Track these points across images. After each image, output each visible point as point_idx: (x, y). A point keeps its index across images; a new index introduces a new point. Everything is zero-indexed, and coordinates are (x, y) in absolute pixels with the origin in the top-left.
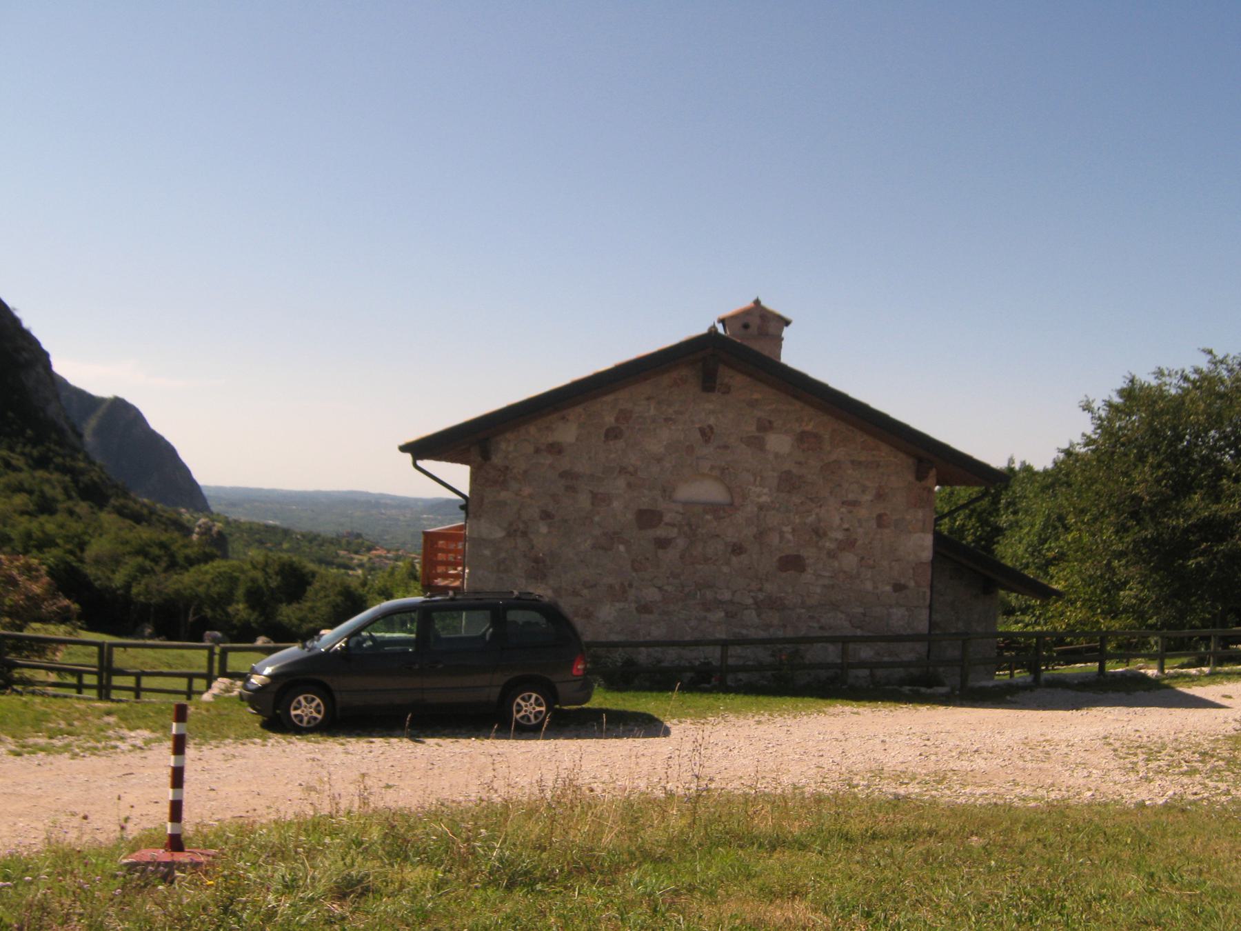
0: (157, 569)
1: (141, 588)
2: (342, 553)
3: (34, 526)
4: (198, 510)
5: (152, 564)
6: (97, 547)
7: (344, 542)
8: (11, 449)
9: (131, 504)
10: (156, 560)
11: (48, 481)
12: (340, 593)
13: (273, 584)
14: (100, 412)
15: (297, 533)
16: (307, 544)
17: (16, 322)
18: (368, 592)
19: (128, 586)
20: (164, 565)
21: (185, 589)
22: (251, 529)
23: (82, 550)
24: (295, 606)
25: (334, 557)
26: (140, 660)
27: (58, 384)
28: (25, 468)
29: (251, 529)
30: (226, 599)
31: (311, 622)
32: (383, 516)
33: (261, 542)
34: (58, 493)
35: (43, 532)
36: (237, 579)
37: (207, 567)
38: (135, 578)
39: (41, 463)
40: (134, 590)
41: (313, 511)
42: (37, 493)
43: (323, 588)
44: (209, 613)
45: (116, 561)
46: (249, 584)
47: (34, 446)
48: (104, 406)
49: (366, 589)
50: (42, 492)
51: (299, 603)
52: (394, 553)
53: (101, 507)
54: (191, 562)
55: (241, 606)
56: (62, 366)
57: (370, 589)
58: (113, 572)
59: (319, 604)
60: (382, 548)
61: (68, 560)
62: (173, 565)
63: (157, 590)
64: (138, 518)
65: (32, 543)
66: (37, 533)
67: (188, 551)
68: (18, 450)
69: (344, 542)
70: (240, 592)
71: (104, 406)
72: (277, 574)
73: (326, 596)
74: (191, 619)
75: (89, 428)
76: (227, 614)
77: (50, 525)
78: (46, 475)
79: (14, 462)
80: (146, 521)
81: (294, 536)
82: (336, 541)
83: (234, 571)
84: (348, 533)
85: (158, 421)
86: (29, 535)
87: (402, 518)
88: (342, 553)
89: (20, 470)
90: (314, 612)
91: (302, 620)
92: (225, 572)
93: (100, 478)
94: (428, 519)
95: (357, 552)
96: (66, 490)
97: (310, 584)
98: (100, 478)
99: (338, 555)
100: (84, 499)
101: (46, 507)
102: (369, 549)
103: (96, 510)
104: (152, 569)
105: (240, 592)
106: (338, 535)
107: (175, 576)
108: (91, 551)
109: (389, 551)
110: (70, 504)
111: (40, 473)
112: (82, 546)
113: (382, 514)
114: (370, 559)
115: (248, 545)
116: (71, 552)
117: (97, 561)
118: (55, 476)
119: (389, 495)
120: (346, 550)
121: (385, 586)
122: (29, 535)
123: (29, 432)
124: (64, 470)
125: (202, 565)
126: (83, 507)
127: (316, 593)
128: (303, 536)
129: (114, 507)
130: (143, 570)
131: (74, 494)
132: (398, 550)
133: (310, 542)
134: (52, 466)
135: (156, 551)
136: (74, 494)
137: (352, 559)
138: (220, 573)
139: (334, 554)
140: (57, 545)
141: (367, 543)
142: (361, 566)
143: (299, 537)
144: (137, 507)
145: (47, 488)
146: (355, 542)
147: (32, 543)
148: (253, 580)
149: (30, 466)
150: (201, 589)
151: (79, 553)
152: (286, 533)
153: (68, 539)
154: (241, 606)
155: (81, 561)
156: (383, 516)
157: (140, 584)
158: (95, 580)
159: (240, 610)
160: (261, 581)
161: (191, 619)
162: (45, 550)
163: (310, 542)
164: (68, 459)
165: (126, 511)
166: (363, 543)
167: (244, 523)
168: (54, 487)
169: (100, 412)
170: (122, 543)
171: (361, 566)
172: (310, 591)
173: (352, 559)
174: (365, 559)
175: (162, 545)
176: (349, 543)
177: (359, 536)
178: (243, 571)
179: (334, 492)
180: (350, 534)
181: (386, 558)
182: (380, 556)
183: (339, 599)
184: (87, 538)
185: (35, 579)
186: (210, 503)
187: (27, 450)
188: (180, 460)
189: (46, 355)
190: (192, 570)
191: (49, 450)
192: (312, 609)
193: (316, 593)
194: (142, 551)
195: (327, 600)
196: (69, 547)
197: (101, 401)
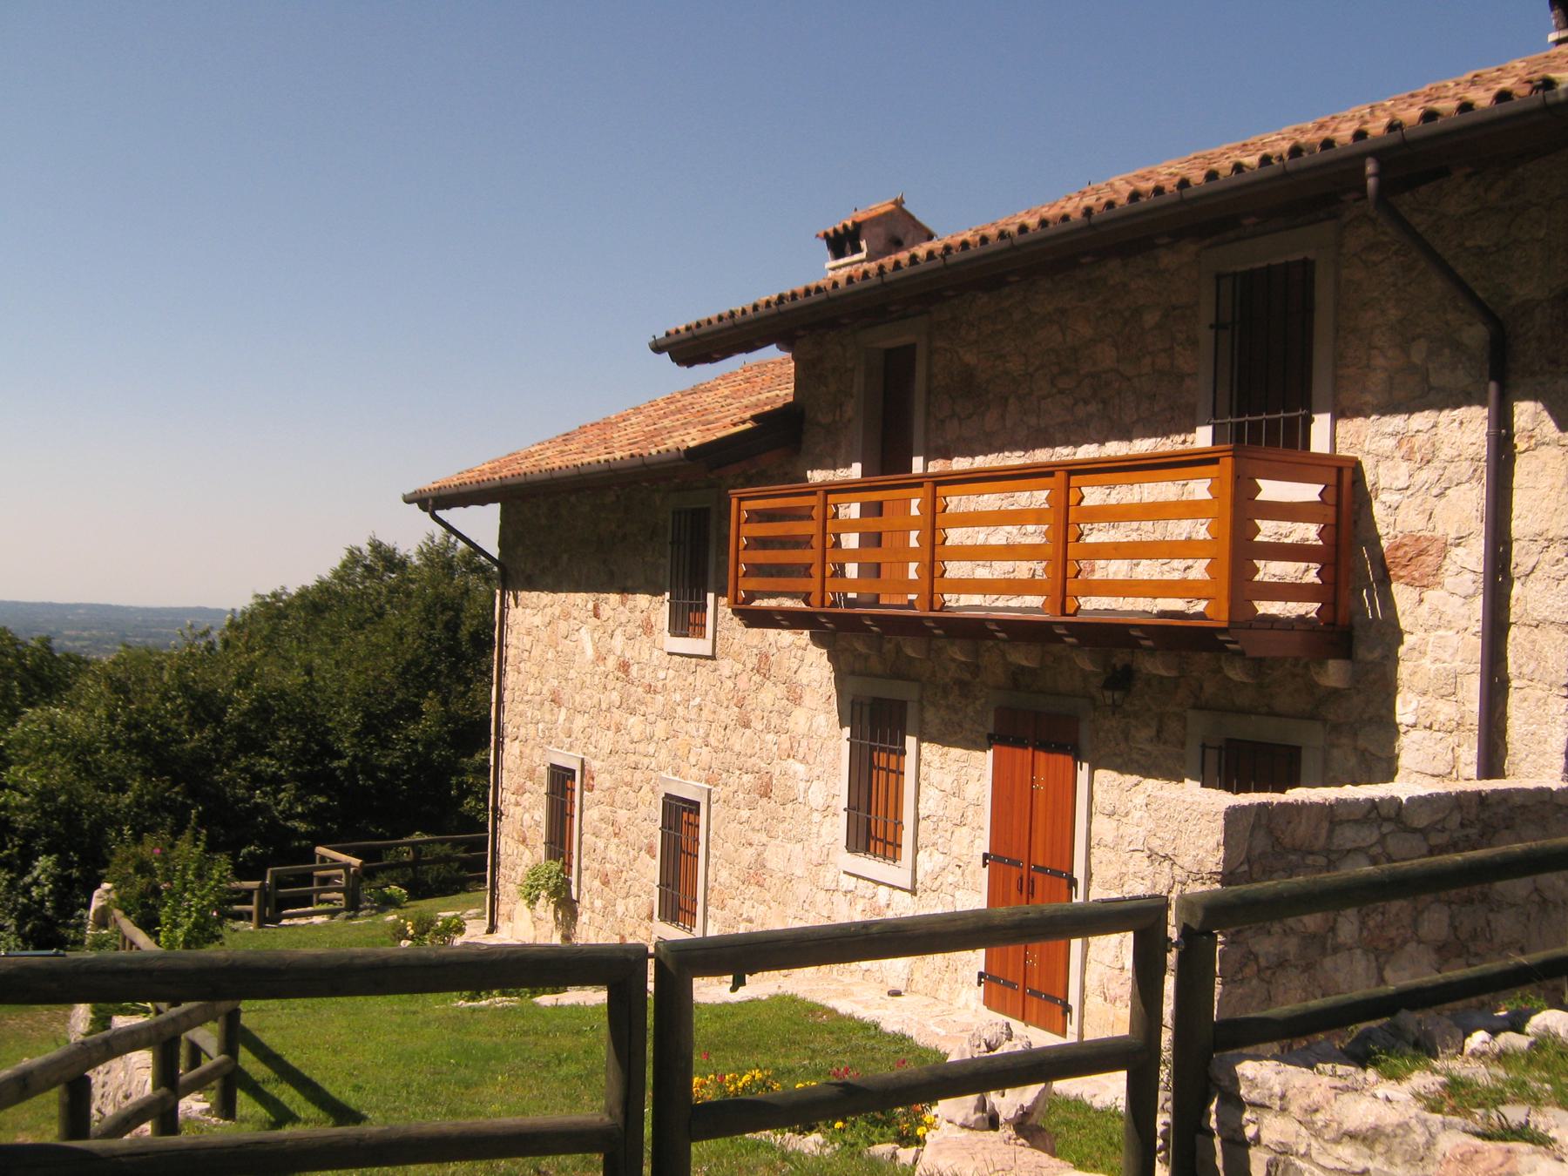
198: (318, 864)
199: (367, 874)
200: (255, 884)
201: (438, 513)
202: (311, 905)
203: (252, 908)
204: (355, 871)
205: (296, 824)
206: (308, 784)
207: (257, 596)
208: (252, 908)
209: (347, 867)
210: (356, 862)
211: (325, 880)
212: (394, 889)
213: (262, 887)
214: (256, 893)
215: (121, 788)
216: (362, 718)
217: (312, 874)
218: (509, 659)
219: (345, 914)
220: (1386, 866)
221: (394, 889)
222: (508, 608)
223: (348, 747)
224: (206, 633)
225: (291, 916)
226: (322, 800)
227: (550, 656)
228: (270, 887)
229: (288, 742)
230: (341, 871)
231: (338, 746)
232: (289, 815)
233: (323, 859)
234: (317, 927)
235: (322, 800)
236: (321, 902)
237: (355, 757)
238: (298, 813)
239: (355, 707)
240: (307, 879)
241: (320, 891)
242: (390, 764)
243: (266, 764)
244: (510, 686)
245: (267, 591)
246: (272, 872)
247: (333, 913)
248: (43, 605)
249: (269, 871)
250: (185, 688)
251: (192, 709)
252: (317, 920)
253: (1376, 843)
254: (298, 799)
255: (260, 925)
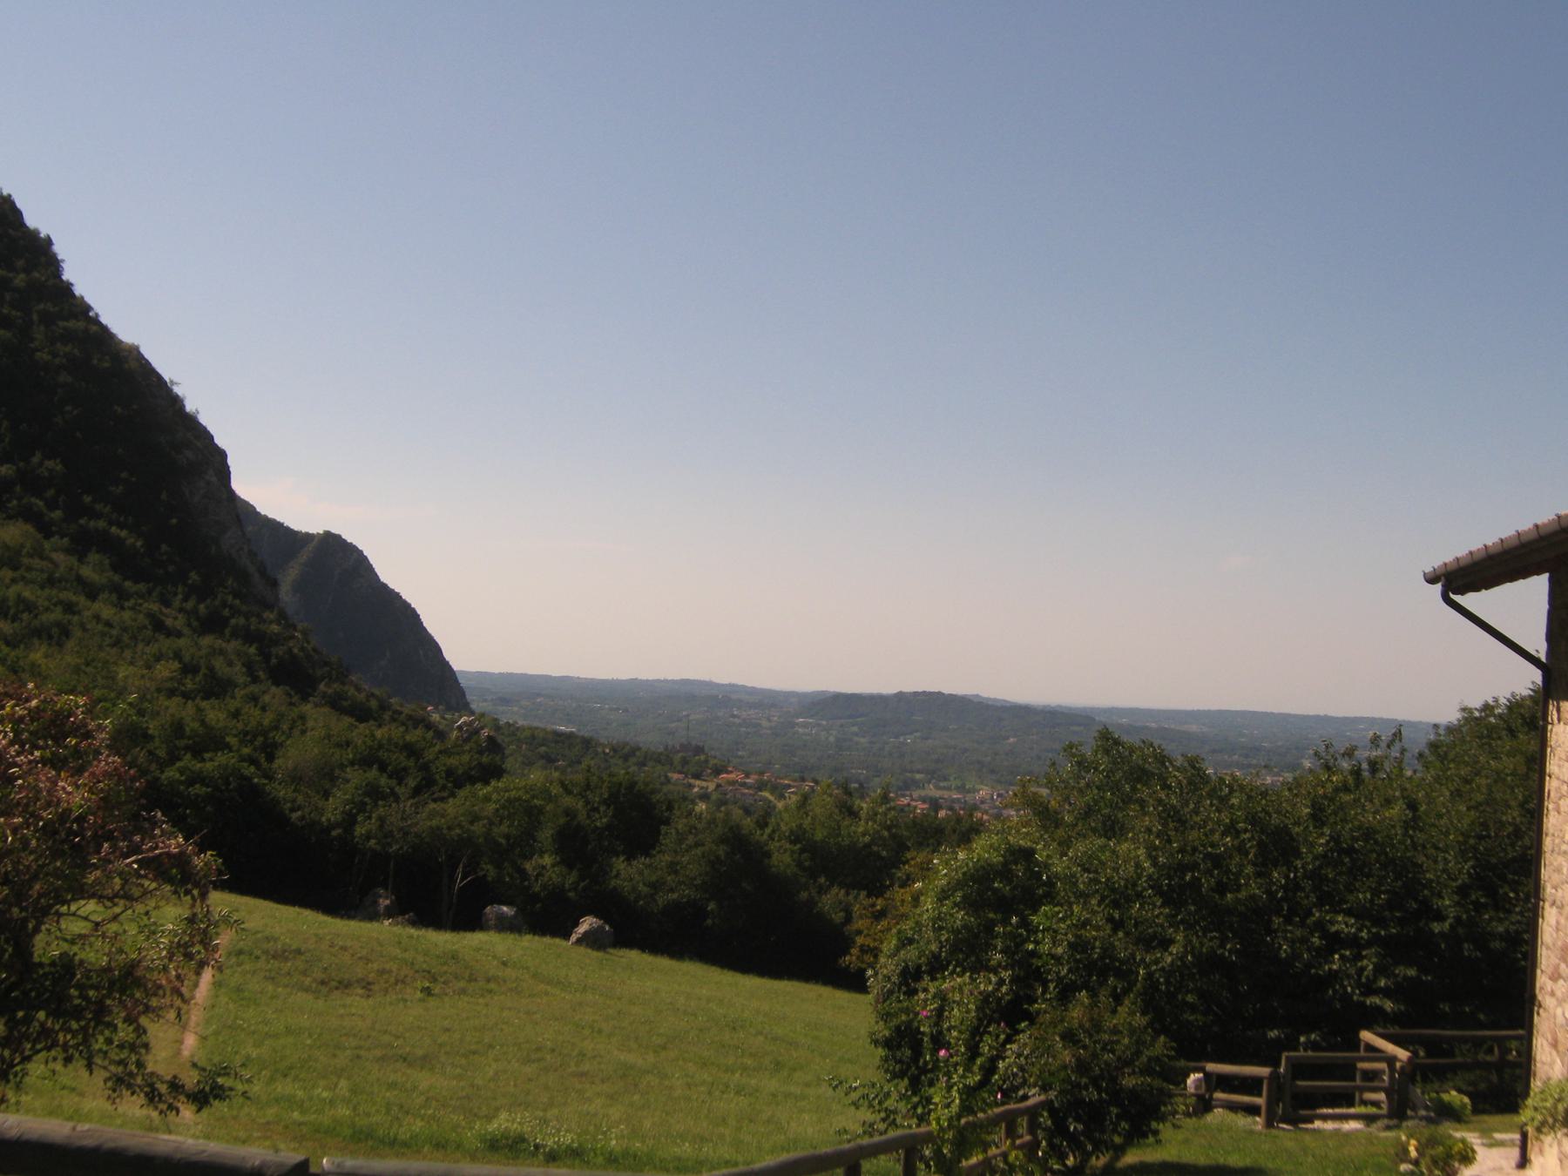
0: (399, 790)
1: (372, 825)
2: (675, 776)
3: (186, 712)
4: (449, 708)
5: (393, 782)
6: (298, 753)
7: (677, 758)
8: (166, 603)
9: (352, 691)
10: (399, 775)
11: (222, 652)
12: (723, 840)
13: (602, 821)
14: (304, 556)
15: (604, 746)
16: (620, 762)
17: (176, 402)
18: (771, 837)
19: (349, 821)
20: (412, 783)
21: (449, 828)
22: (533, 737)
23: (271, 758)
24: (642, 861)
25: (662, 784)
26: (375, 966)
27: (243, 513)
28: (186, 631)
29: (533, 737)
30: (524, 843)
31: (672, 890)
32: (736, 720)
33: (550, 760)
34: (237, 673)
35: (203, 722)
36: (541, 810)
37: (483, 791)
38: (361, 807)
39: (212, 624)
40: (359, 830)
41: (626, 711)
42: (203, 671)
43: (692, 829)
44: (489, 870)
45: (327, 777)
46: (562, 821)
47: (201, 600)
48: (311, 547)
49: (768, 831)
50: (211, 669)
51: (647, 855)
52: (756, 777)
53: (305, 698)
54: (458, 780)
55: (547, 860)
56: (242, 485)
57: (774, 831)
58: (326, 795)
59: (685, 859)
60: (736, 768)
61: (246, 772)
62: (426, 785)
63: (401, 829)
64: (361, 714)
65: (182, 743)
66: (192, 725)
67: (453, 761)
68: (177, 602)
69: (677, 758)
70: (546, 835)
71: (311, 547)
72: (606, 802)
73: (697, 845)
74: (459, 884)
75: (288, 577)
76: (522, 873)
77: (215, 714)
78: (219, 643)
79: (169, 622)
80: (375, 720)
81: (600, 750)
82: (663, 758)
83: (534, 797)
84: (682, 745)
85: (392, 571)
86: (178, 728)
87: (765, 723)
88: (675, 776)
89: (179, 635)
90: (676, 872)
91: (656, 886)
92: (519, 799)
93: (302, 649)
94: (805, 725)
95: (697, 776)
96: (249, 667)
97: (667, 822)
98: (302, 649)
99: (668, 781)
100: (277, 684)
101: (216, 688)
102: (717, 771)
103: (295, 699)
104: (393, 793)
105: (546, 835)
106: (666, 748)
107: (432, 805)
108: (284, 763)
109: (747, 776)
110: (254, 688)
111: (207, 641)
112: (270, 751)
113: (734, 716)
114: (719, 786)
115: (529, 763)
116: (253, 761)
117: (296, 778)
118: (234, 645)
119: (744, 687)
120: (680, 772)
121: (800, 826)
122: (178, 728)
123: (194, 576)
124: (249, 637)
125: (478, 786)
126: (275, 695)
127: (681, 839)
128: (614, 750)
129: (324, 695)
130: (374, 793)
131: (261, 674)
132: (762, 773)
133: (626, 758)
134: (227, 631)
135: (400, 759)
136: (261, 674)
137: (691, 786)
138: (509, 801)
139: (663, 778)
140: (228, 747)
141: (712, 762)
142: (705, 797)
143: (607, 751)
144: (362, 697)
145: (218, 663)
146: (695, 760)
147: (182, 743)
148: (569, 813)
149: (195, 631)
150: (478, 828)
151: (265, 765)
152: (587, 743)
153: (246, 736)
154: (547, 860)
155: (270, 778)
156: (736, 720)
157: (370, 818)
158: (293, 810)
159: (545, 865)
160: (582, 817)
161: (459, 884)
162: (207, 756)
163: (626, 758)
164: (253, 620)
165: (345, 704)
166: (706, 761)
167: (523, 729)
168: (230, 664)
169: (304, 556)
170: (339, 745)
171: (705, 797)
172: (668, 836)
173: (691, 786)
174: (712, 786)
175: (411, 750)
176: (685, 762)
177: (699, 750)
178: (550, 798)
179: (659, 681)
180: (684, 747)
181: (744, 785)
182: (733, 783)
183: (722, 851)
184: (279, 738)
185: (75, 763)
186: (469, 697)
187: (189, 605)
188: (425, 629)
189: (222, 455)
190: (462, 793)
191: (224, 604)
192: (673, 868)
193: (681, 839)
194: (367, 761)
195: (699, 851)
196: (246, 751)
197: (308, 537)
198: (1362, 1053)
199: (1413, 1072)
200: (1263, 1071)
201: (1468, 600)
202: (1351, 1104)
203: (1260, 1101)
204: (1402, 1068)
205: (1378, 1001)
206: (1394, 950)
207: (1464, 710)
208: (1260, 1101)
209: (1391, 1060)
210: (1403, 1054)
211: (1370, 1076)
212: (1453, 1097)
213: (1274, 1077)
214: (1265, 1082)
215: (1166, 943)
216: (1473, 867)
217: (1355, 1065)
218: (1552, 794)
219: (1386, 1121)
220: (1310, 1053)
221: (1453, 1097)
222: (1552, 724)
223: (1450, 906)
224: (1349, 753)
225: (1325, 1118)
226: (1412, 972)
227: (1275, 770)
228: (1284, 1077)
229: (1369, 896)
230: (1383, 1066)
231: (1437, 903)
232: (1369, 990)
233: (1370, 1048)
234: (1348, 1134)
235: (1412, 972)
236: (1364, 1103)
237: (1458, 919)
238: (1381, 988)
239: (1463, 853)
240: (1347, 1071)
241: (1362, 1090)
242: (1507, 931)
243: (1342, 924)
244: (1551, 831)
245: (1476, 703)
246: (1287, 1057)
247: (1369, 1119)
248: (1317, 718)
249: (1284, 1055)
250: (1253, 820)
251: (1260, 844)
252: (1353, 1125)
253: (93, 922)
254: (1380, 970)
255: (1269, 1124)
